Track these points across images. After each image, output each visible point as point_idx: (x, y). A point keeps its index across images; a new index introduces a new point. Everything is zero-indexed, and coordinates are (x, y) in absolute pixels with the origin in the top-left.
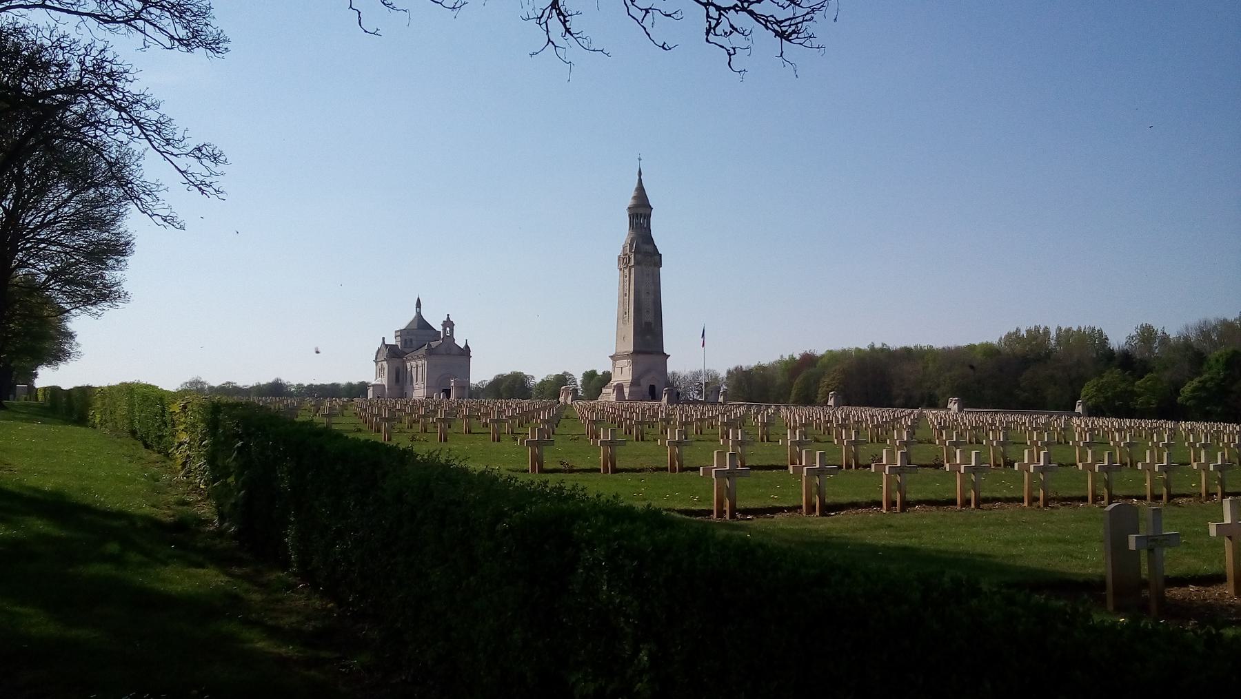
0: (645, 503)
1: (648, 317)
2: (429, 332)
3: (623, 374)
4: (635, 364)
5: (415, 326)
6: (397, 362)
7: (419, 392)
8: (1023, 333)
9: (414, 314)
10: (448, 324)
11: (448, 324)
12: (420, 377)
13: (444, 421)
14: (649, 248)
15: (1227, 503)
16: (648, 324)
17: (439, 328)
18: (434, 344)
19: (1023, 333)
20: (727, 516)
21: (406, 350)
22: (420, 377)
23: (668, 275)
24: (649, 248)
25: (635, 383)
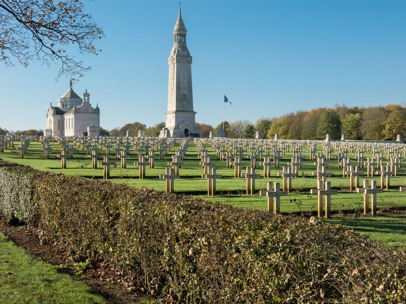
0: (293, 210)
1: (186, 92)
2: (79, 99)
3: (171, 123)
4: (177, 117)
5: (69, 96)
6: (58, 117)
7: (69, 132)
8: (289, 114)
9: (69, 89)
10: (87, 95)
11: (87, 95)
12: (71, 125)
13: (147, 141)
14: (185, 53)
15: (252, 174)
16: (185, 95)
17: (82, 97)
18: (78, 107)
19: (289, 114)
20: (326, 216)
21: (64, 110)
22: (71, 125)
23: (194, 67)
24: (185, 53)
25: (176, 128)
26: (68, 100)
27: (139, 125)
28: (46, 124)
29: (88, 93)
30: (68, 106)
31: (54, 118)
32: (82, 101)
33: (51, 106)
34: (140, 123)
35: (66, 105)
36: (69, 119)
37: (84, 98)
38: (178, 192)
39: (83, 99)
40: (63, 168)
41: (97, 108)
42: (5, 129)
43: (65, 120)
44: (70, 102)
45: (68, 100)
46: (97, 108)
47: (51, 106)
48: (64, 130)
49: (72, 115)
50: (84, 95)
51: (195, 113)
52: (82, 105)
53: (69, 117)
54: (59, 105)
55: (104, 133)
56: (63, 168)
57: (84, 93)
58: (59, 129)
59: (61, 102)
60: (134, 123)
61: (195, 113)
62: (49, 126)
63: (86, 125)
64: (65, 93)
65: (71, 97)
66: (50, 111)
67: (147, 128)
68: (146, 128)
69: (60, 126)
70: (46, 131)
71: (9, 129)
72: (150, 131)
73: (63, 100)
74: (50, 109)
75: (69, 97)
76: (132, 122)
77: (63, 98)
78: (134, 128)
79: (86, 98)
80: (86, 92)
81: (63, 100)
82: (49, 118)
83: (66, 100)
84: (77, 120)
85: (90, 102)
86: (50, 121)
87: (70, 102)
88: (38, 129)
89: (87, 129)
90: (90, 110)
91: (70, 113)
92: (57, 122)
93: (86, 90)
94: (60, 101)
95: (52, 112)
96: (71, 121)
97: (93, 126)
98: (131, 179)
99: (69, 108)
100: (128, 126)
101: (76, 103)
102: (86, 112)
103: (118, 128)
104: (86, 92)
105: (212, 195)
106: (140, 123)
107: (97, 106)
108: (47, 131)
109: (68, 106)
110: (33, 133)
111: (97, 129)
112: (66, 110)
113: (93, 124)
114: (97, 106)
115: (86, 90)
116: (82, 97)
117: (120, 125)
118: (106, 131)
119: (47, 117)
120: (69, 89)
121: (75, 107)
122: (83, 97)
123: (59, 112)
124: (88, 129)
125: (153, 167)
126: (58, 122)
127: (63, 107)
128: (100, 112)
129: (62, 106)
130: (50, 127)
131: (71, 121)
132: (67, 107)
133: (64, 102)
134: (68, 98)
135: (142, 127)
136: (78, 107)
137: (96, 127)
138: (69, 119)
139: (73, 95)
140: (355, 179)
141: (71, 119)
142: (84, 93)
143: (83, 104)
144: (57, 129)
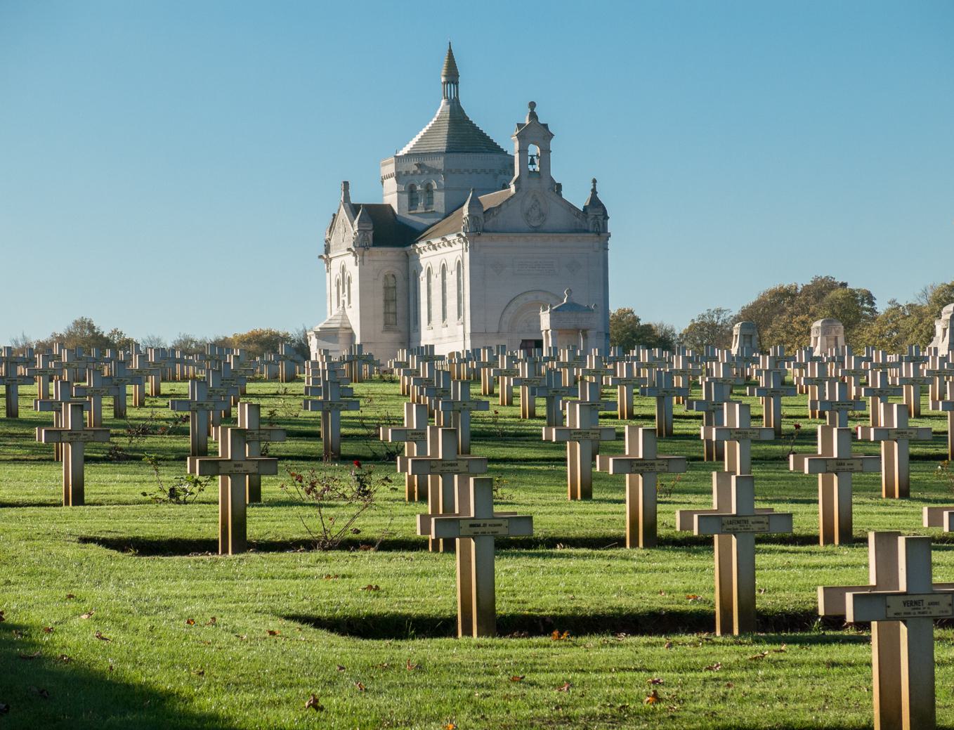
2: (496, 157)
5: (440, 143)
6: (386, 257)
11: (536, 132)
18: (490, 200)
21: (416, 220)
26: (439, 163)
27: (833, 293)
28: (329, 298)
29: (541, 121)
30: (439, 198)
31: (362, 261)
32: (512, 166)
33: (347, 198)
34: (839, 280)
35: (429, 190)
36: (444, 268)
37: (523, 151)
38: (554, 617)
39: (517, 156)
40: (67, 504)
41: (595, 202)
42: (115, 332)
43: (423, 275)
44: (447, 172)
45: (439, 163)
46: (595, 202)
47: (347, 198)
48: (418, 331)
49: (459, 246)
50: (520, 137)
51: (550, 152)
52: (513, 189)
53: (444, 259)
54: (390, 195)
55: (636, 335)
56: (67, 504)
57: (520, 126)
58: (388, 327)
59: (399, 176)
60: (808, 281)
61: (550, 152)
62: (335, 312)
63: (531, 297)
64: (424, 128)
65: (452, 149)
66: (339, 228)
67: (881, 307)
68: (873, 311)
69: (398, 304)
70: (318, 335)
71: (138, 334)
72: (896, 329)
73: (412, 166)
74: (343, 214)
75: (443, 148)
76: (800, 279)
77: (408, 156)
78: (804, 310)
79: (534, 150)
80: (533, 116)
81: (412, 166)
82: (336, 265)
83: (428, 163)
84: (483, 273)
85: (557, 174)
86: (344, 282)
87: (447, 172)
88: (289, 326)
89: (539, 321)
90: (557, 218)
91: (449, 238)
92: (380, 285)
93: (532, 105)
94: (391, 169)
95: (348, 230)
96: (451, 278)
97: (572, 307)
98: (371, 552)
99: (442, 210)
100: (774, 305)
101: (482, 181)
102: (536, 230)
103: (719, 311)
104: (533, 116)
105: (736, 632)
106: (844, 285)
107: (594, 191)
108: (324, 334)
109: (439, 198)
110: (267, 343)
111: (596, 322)
112: (427, 222)
113: (570, 292)
114: (594, 191)
115: (532, 105)
116: (512, 146)
117: (732, 298)
118: (659, 333)
119: (328, 261)
120: (443, 102)
121: (475, 204)
122: (517, 145)
123: (387, 233)
124: (545, 320)
125: (587, 495)
126: (386, 288)
127: (413, 202)
128: (611, 226)
129: (406, 196)
130: (344, 316)
131: (451, 278)
132: (430, 201)
133: (413, 177)
134: (438, 154)
135: (849, 310)
136: (490, 200)
137: (588, 309)
138: (444, 268)
139: (465, 136)
140: (566, 421)
141: (452, 267)
142: (520, 126)
143: (517, 182)
144: (381, 322)
